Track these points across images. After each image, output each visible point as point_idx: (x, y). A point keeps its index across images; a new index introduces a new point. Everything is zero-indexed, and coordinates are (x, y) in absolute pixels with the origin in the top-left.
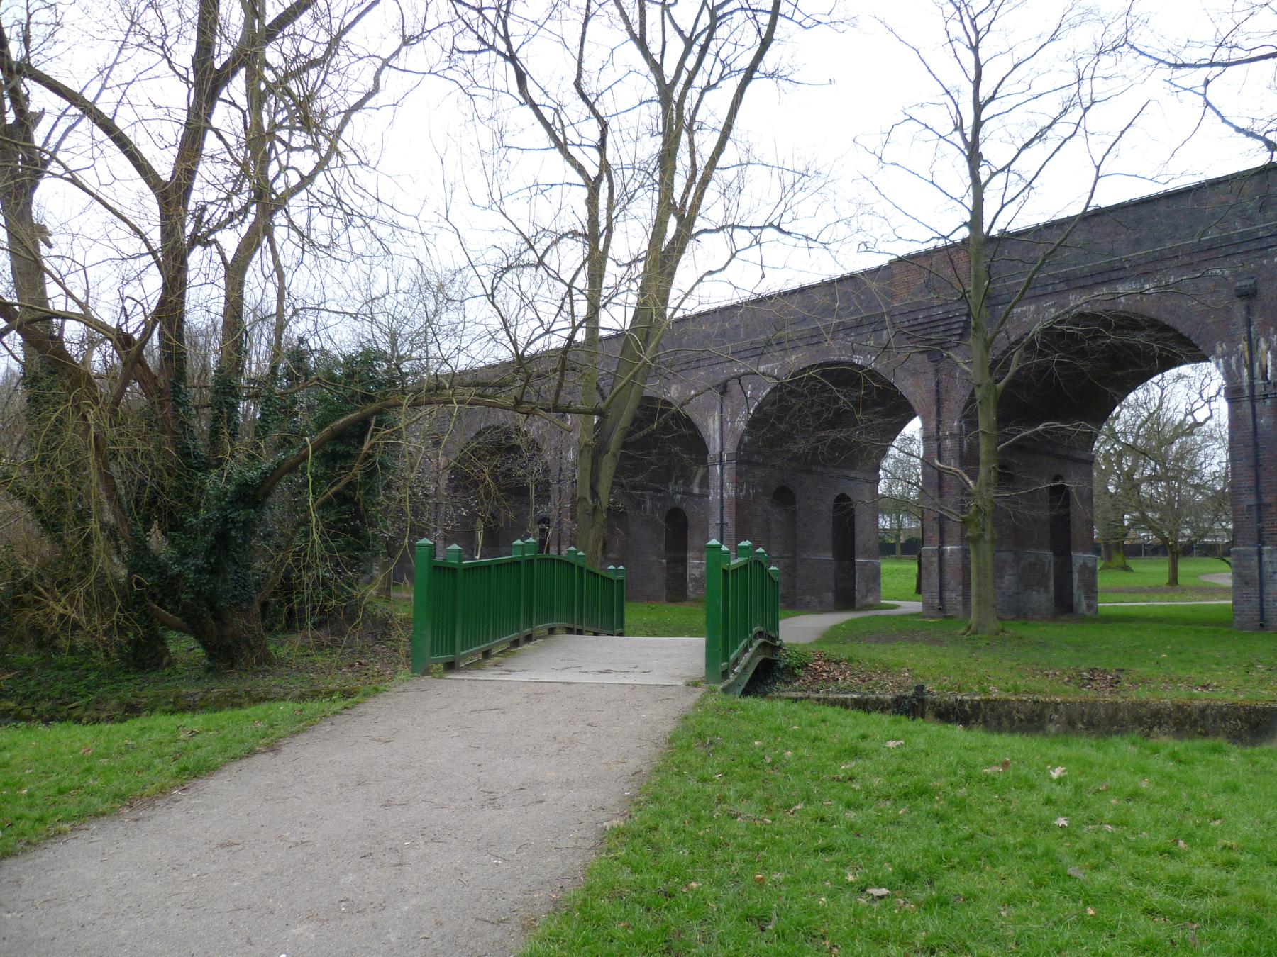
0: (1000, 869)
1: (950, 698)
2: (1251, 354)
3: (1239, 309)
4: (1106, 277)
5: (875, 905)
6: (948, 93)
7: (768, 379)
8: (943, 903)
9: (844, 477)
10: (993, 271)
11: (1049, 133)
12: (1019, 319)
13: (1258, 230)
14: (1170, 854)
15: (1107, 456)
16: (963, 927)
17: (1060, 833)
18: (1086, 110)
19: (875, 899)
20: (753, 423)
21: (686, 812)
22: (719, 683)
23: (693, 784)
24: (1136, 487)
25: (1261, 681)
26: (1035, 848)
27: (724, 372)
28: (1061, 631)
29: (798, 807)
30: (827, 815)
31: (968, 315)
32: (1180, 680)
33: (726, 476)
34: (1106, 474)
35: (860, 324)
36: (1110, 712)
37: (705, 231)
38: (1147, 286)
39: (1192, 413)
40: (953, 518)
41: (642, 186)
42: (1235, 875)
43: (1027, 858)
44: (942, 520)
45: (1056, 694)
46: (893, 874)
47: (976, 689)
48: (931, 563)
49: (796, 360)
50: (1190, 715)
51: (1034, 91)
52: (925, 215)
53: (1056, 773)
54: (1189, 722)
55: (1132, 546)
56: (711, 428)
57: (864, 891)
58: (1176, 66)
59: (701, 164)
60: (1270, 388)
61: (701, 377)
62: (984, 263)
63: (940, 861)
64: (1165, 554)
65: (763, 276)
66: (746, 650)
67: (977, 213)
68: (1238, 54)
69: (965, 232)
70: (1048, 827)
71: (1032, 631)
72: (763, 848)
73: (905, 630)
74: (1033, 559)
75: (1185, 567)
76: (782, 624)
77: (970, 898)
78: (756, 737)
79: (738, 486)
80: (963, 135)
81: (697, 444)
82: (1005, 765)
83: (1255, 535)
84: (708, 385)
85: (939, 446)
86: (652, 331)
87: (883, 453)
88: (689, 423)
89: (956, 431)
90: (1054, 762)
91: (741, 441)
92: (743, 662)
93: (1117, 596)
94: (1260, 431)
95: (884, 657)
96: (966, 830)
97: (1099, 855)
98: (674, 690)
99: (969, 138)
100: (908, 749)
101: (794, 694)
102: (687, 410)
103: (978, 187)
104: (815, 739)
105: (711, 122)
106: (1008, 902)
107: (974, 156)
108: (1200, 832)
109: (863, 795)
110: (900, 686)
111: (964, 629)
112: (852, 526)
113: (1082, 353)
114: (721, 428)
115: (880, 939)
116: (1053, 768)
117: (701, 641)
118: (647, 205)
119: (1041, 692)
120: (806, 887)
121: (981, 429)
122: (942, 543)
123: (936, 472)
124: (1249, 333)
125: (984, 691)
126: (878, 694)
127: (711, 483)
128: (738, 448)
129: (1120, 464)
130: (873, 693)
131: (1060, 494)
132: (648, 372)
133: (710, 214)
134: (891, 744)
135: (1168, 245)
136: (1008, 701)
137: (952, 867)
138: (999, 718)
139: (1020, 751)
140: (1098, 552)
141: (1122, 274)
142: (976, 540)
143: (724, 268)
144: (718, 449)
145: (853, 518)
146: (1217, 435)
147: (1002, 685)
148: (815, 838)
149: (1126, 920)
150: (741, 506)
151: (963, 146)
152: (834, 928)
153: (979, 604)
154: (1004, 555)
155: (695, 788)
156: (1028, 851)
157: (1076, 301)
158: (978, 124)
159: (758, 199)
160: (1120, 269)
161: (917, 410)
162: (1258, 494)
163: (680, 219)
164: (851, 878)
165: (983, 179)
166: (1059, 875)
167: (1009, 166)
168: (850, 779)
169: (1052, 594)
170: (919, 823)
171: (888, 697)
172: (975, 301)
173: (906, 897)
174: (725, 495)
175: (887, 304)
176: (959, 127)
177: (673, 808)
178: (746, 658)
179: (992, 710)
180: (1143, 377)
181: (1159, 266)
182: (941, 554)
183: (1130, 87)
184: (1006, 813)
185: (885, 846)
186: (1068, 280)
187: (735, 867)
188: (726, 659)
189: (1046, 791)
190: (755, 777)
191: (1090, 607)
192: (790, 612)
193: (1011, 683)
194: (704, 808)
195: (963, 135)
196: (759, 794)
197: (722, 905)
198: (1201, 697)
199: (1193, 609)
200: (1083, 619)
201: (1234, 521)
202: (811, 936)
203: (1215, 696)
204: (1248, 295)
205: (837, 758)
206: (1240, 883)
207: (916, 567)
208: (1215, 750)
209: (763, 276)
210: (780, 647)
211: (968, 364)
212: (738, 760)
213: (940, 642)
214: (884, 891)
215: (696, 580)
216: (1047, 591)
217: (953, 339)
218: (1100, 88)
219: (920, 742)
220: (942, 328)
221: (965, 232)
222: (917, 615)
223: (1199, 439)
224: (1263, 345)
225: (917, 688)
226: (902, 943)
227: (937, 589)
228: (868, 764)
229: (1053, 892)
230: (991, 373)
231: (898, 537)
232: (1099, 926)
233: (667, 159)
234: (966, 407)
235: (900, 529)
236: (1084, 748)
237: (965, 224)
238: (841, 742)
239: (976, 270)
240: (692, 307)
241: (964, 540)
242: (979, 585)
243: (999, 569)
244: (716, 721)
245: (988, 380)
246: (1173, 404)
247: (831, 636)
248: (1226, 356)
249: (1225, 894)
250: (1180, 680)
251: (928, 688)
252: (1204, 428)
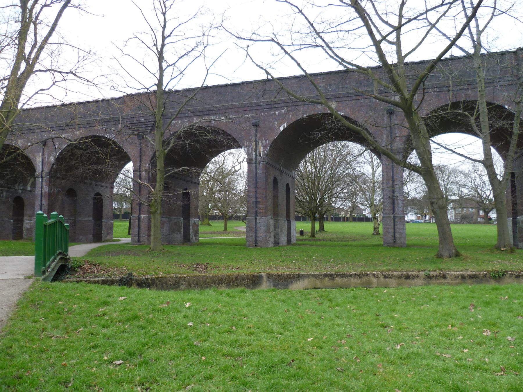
0: (168, 346)
1: (143, 277)
2: (256, 147)
3: (253, 129)
4: (208, 113)
5: (117, 368)
6: (152, 30)
7: (67, 141)
8: (146, 363)
9: (99, 185)
10: (165, 105)
11: (190, 54)
12: (174, 125)
13: (261, 102)
14: (230, 332)
15: (204, 182)
16: (155, 372)
17: (190, 328)
18: (205, 47)
19: (117, 365)
20: (58, 160)
21: (26, 338)
22: (41, 276)
23: (30, 324)
24: (214, 194)
25: (256, 265)
26: (181, 336)
27: (45, 136)
28: (186, 249)
29: (81, 330)
30: (95, 332)
31: (155, 122)
32: (229, 266)
33: (44, 183)
34: (203, 188)
35: (109, 121)
36: (204, 279)
37: (40, 71)
38: (222, 118)
39: (234, 167)
40: (145, 204)
41: (9, 44)
42: (253, 337)
43: (178, 340)
44: (140, 204)
45: (184, 274)
46: (124, 354)
47: (153, 273)
48: (135, 222)
49: (79, 133)
50: (232, 279)
51: (186, 36)
52: (139, 79)
53: (187, 305)
54: (232, 282)
55: (211, 216)
56: (38, 161)
57: (112, 363)
58: (238, 38)
59: (40, 41)
60: (262, 160)
61: (35, 137)
62: (160, 103)
63: (143, 346)
64: (223, 219)
65: (66, 95)
66: (53, 261)
67: (160, 81)
68: (259, 38)
69: (155, 88)
70: (186, 327)
71: (175, 249)
72: (65, 350)
73: (124, 250)
74: (175, 221)
75: (229, 224)
76: (70, 248)
77: (156, 360)
78: (60, 300)
79: (50, 187)
80: (157, 48)
81: (30, 167)
82: (168, 303)
83: (255, 213)
84: (38, 141)
85: (140, 175)
86: (10, 115)
87: (116, 176)
88: (27, 158)
89: (147, 168)
90: (186, 300)
91: (52, 167)
92: (52, 266)
93: (206, 235)
94: (258, 175)
95: (115, 261)
96: (154, 331)
97: (205, 335)
98: (19, 281)
99: (159, 50)
100: (128, 300)
101: (75, 280)
102: (26, 153)
103: (162, 71)
104: (87, 299)
105: (46, 21)
106: (172, 359)
107: (161, 58)
108: (240, 323)
109: (109, 322)
110: (122, 273)
111: (148, 249)
112: (102, 207)
113: (198, 141)
114: (42, 161)
115: (120, 383)
116: (186, 303)
117: (33, 258)
118: (12, 53)
119: (178, 273)
120: (86, 365)
121: (158, 168)
122: (140, 214)
123: (138, 185)
124: (256, 139)
125: (157, 274)
126: (113, 277)
127: (37, 186)
128: (50, 171)
129: (208, 185)
130: (111, 277)
131: (187, 195)
132: (7, 133)
133: (43, 63)
134: (121, 298)
135: (230, 103)
136: (165, 277)
137: (149, 348)
138: (162, 284)
139: (173, 297)
140: (199, 218)
141: (214, 112)
142: (154, 213)
143: (48, 89)
144: (40, 171)
145: (102, 203)
146: (242, 175)
147: (164, 271)
148: (89, 343)
149: (216, 360)
150: (50, 196)
151: (157, 53)
152: (99, 381)
153: (154, 239)
154: (164, 219)
155: (31, 326)
156: (178, 337)
157: (196, 121)
158: (163, 45)
159: (67, 60)
160: (213, 110)
161: (131, 158)
162: (256, 198)
163: (27, 63)
164: (106, 358)
165: (164, 68)
166: (191, 346)
167: (174, 64)
168: (104, 315)
169: (182, 235)
170: (134, 331)
171: (117, 278)
172: (158, 116)
173: (130, 362)
174: (43, 191)
175: (121, 114)
176: (156, 45)
177: (20, 336)
178: (54, 264)
179: (160, 281)
180: (217, 153)
181: (227, 111)
182: (139, 218)
183: (221, 42)
184: (169, 323)
185: (120, 342)
186: (193, 112)
187: (52, 360)
188: (45, 265)
189: (184, 313)
190: (60, 318)
191: (196, 239)
192: (72, 244)
193: (167, 270)
194: (36, 335)
195: (157, 48)
196: (62, 325)
197: (46, 379)
198: (236, 272)
199: (233, 240)
200: (193, 244)
201: (247, 208)
202: (89, 386)
203: (241, 271)
204: (256, 125)
205: (98, 306)
206: (255, 340)
207: (128, 224)
208: (242, 292)
209: (66, 95)
210: (69, 259)
211: (153, 141)
212: (52, 311)
213: (139, 255)
214: (121, 362)
215: (27, 229)
216: (180, 233)
217: (148, 131)
218: (211, 41)
219: (133, 296)
220: (143, 126)
221: (155, 88)
222: (129, 244)
223: (236, 177)
224: (260, 144)
225: (129, 274)
226: (130, 383)
227: (137, 233)
228: (111, 308)
229: (189, 353)
230: (163, 146)
231: (121, 211)
232: (207, 363)
233: (23, 34)
234: (152, 159)
235: (122, 208)
236: (195, 294)
237: (156, 84)
238: (99, 299)
239: (159, 103)
240: (32, 105)
241: (149, 213)
242: (155, 231)
243: (163, 224)
244: (40, 294)
245: (161, 149)
246: (228, 163)
247: (91, 253)
248: (248, 147)
249: (250, 345)
250: (229, 266)
251: (134, 274)
252: (238, 173)
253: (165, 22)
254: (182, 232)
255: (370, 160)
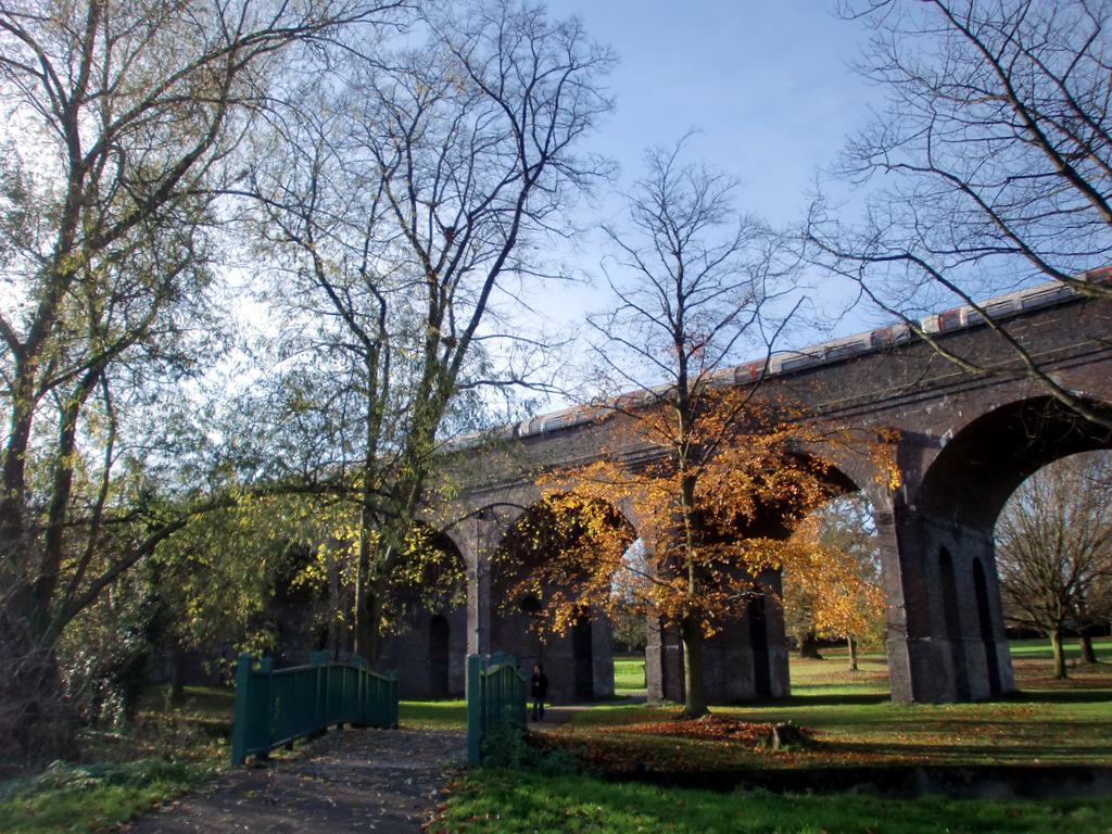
158: (682, 310)
253: (681, 267)
254: (753, 677)
255: (1002, 90)
